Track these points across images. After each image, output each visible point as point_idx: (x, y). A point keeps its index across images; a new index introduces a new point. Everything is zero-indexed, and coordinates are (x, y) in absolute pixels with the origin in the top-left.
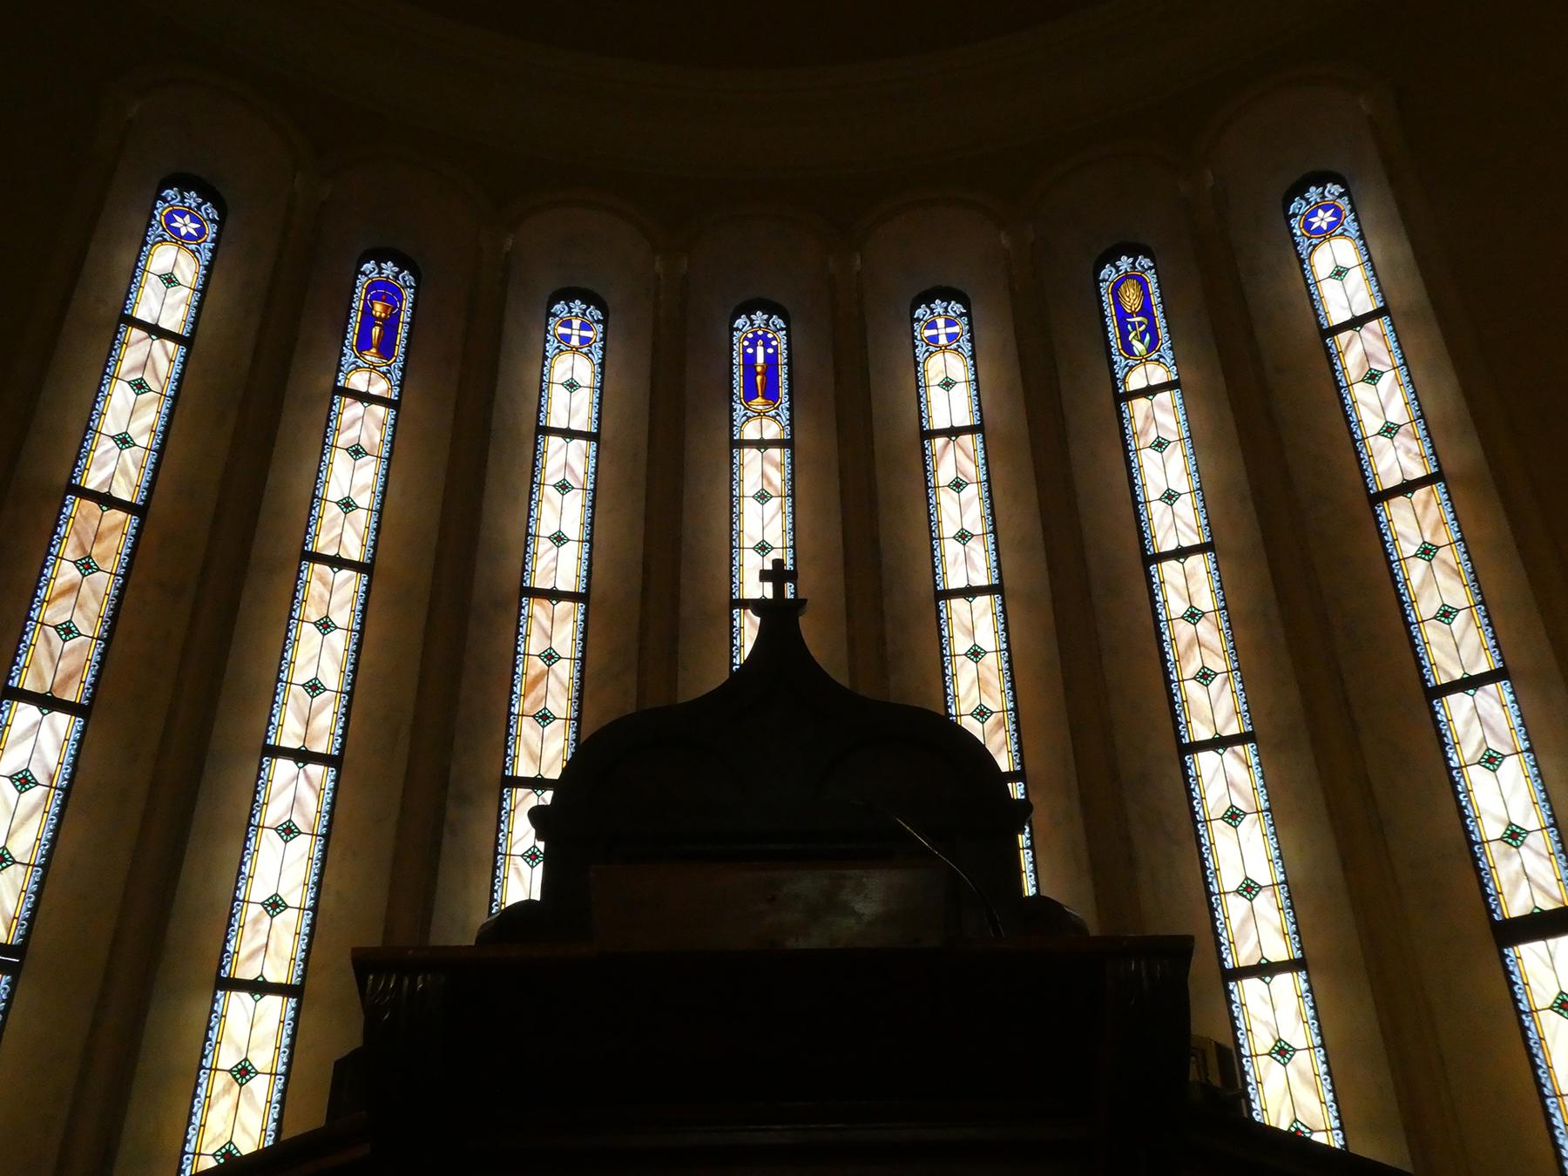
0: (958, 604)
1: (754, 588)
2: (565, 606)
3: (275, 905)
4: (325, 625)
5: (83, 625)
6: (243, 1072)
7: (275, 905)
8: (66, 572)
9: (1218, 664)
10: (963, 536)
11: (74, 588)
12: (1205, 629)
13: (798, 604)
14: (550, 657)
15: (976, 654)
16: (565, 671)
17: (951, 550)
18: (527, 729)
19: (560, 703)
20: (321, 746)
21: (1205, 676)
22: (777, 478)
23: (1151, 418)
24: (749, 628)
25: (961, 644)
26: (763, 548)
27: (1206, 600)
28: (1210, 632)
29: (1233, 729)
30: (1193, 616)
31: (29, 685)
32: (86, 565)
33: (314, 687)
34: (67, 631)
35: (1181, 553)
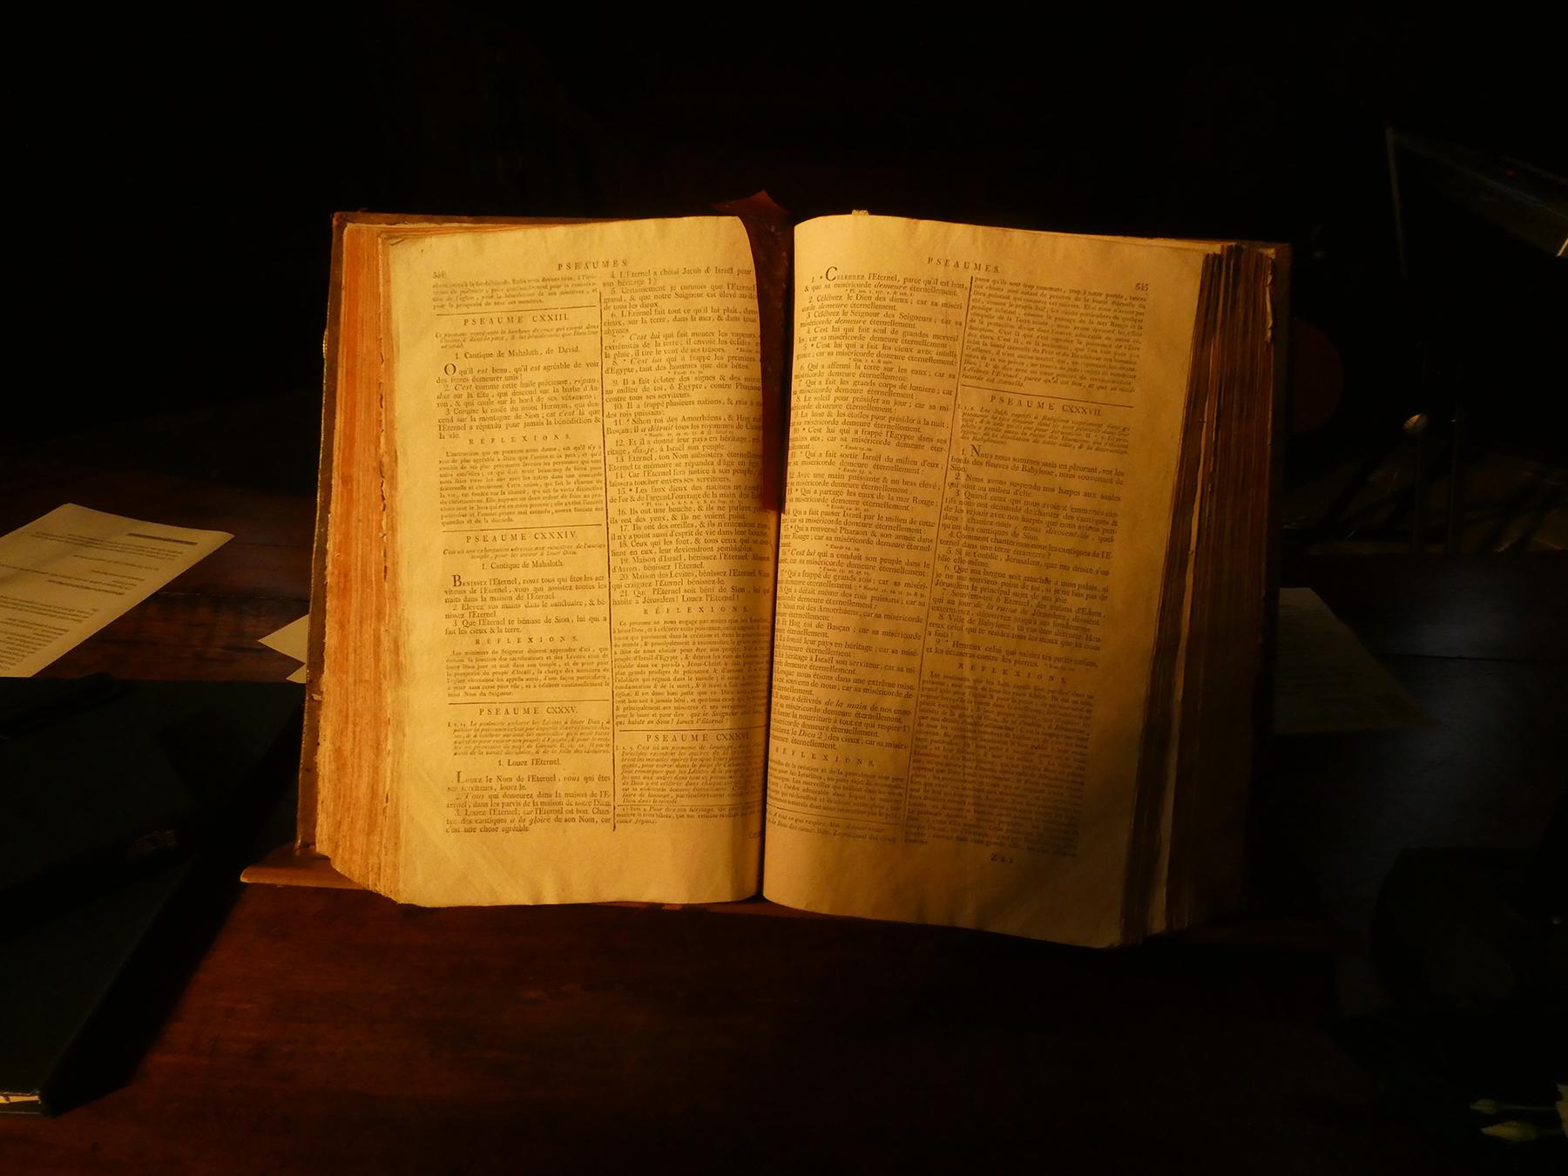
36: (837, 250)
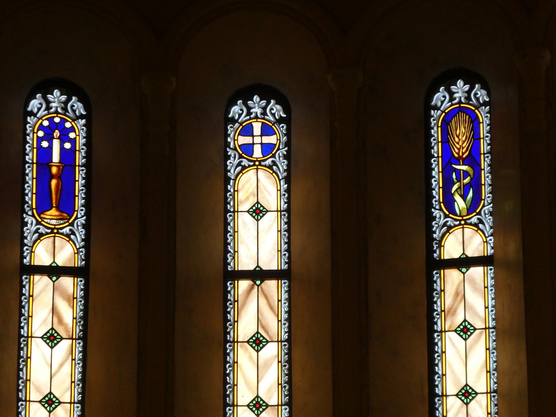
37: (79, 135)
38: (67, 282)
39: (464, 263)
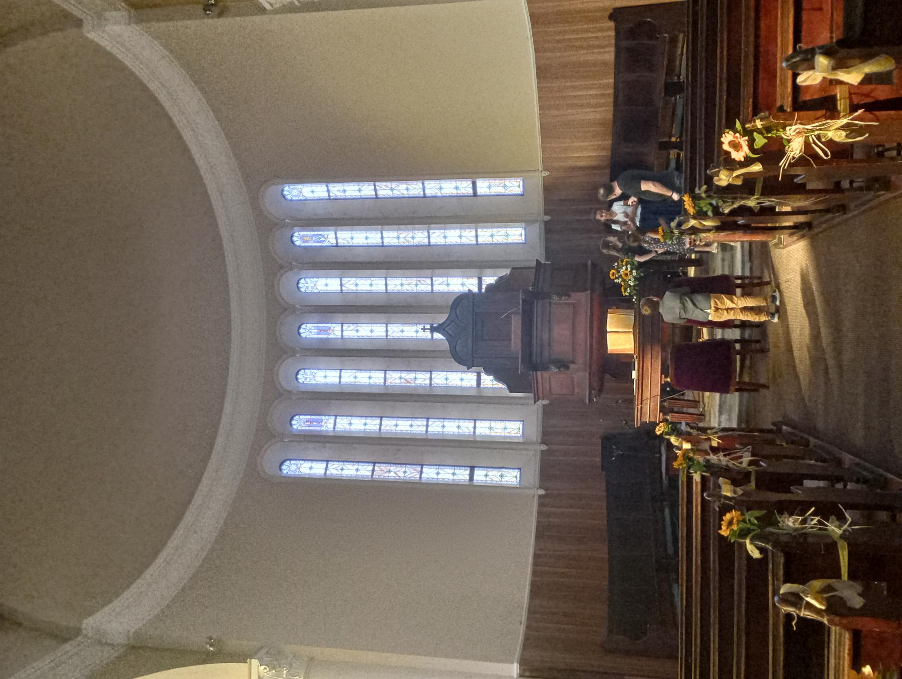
0: (389, 288)
1: (428, 334)
2: (388, 376)
3: (459, 427)
4: (396, 425)
5: (404, 469)
6: (490, 428)
7: (459, 427)
8: (392, 474)
9: (411, 235)
10: (371, 285)
11: (395, 473)
12: (402, 236)
13: (432, 325)
14: (401, 378)
15: (402, 285)
16: (404, 375)
17: (374, 288)
18: (418, 382)
19: (412, 375)
20: (425, 423)
21: (413, 238)
22: (352, 327)
23: (344, 239)
24: (437, 335)
25: (399, 288)
26: (417, 331)
27: (395, 234)
28: (403, 235)
29: (426, 234)
30: (398, 238)
31: (418, 476)
32: (390, 471)
33: (411, 426)
34: (405, 472)
35: (382, 238)
36: (608, 329)
37: (310, 326)
38: (344, 328)
39: (336, 238)
